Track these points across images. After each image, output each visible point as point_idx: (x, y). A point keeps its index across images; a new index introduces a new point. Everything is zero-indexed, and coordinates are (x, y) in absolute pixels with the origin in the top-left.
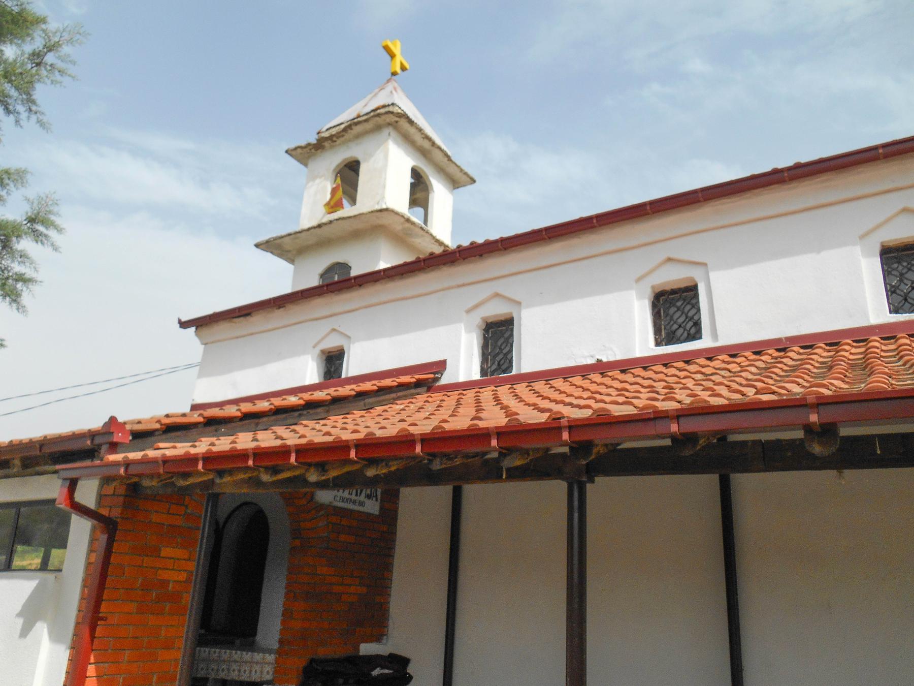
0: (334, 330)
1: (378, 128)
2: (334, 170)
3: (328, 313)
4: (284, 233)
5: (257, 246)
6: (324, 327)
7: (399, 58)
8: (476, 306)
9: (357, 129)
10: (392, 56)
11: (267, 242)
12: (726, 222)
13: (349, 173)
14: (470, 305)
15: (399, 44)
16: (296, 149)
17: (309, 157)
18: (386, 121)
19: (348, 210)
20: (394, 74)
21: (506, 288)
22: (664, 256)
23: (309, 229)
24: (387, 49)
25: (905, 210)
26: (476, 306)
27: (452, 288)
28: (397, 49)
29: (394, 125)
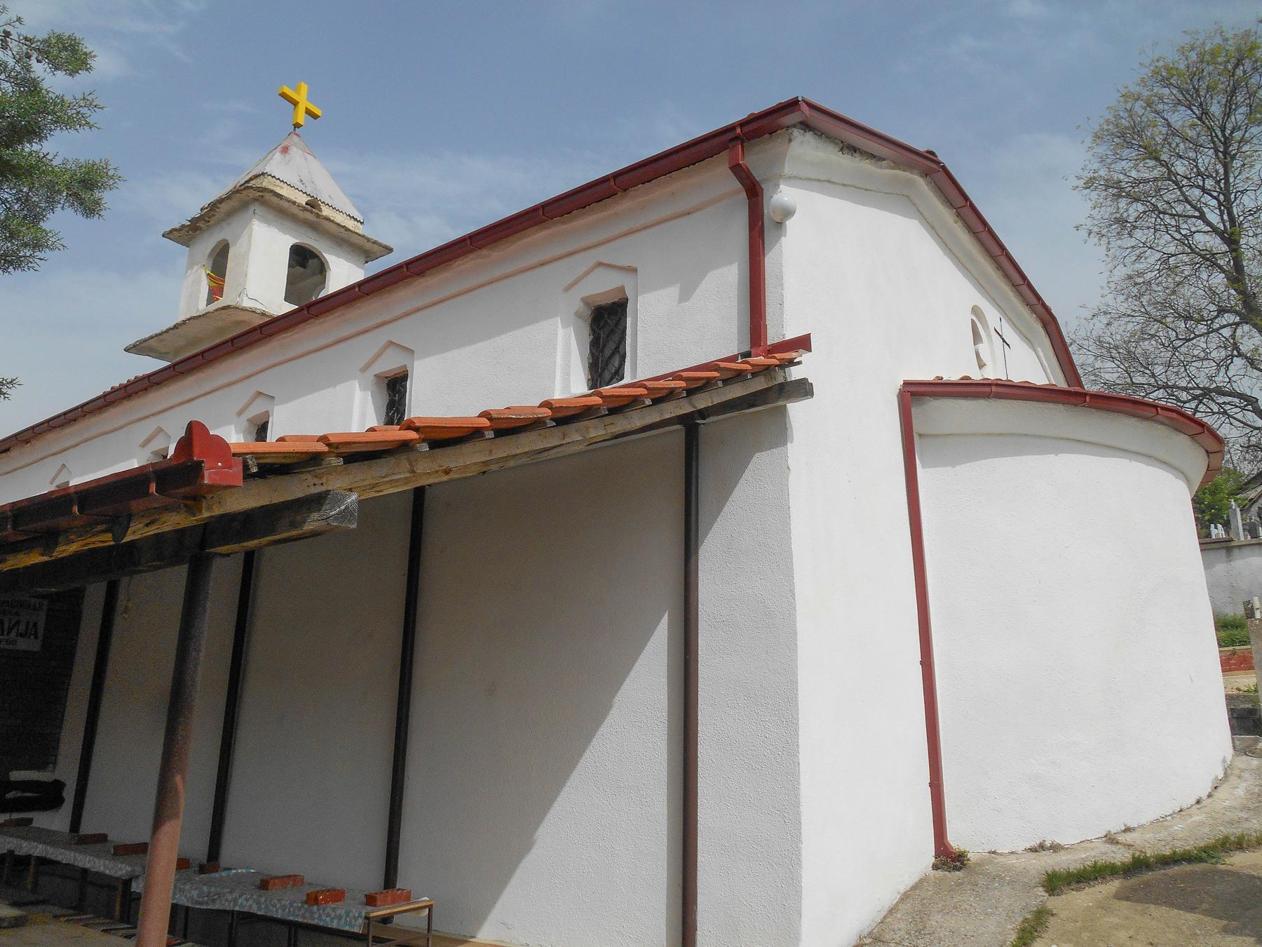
0: (391, 343)
1: (244, 206)
2: (210, 254)
3: (59, 449)
4: (147, 336)
5: (127, 350)
6: (368, 345)
7: (304, 103)
8: (148, 441)
9: (224, 207)
10: (295, 103)
11: (134, 346)
12: (292, 354)
13: (219, 262)
14: (571, 280)
15: (304, 88)
16: (171, 232)
17: (190, 240)
18: (252, 197)
19: (222, 302)
20: (297, 126)
21: (619, 253)
22: (252, 392)
23: (167, 331)
24: (284, 95)
25: (600, 264)
26: (148, 441)
27: (133, 422)
28: (302, 97)
29: (261, 201)
